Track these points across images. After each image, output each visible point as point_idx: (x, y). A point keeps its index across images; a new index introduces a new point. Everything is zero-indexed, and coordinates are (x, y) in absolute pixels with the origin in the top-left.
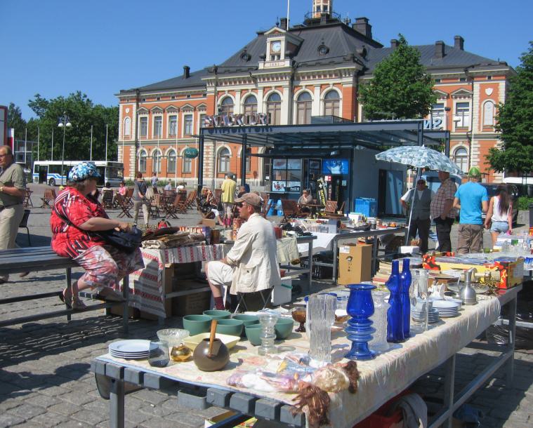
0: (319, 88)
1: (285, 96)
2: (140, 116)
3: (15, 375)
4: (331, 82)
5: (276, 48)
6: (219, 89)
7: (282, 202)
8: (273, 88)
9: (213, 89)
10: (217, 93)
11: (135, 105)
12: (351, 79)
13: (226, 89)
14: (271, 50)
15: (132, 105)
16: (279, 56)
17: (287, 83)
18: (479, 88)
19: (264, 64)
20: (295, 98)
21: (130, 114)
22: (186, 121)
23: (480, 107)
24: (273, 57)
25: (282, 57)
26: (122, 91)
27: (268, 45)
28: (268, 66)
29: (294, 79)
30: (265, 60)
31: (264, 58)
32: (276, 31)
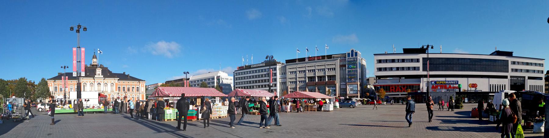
5: (99, 73)
11: (53, 83)
16: (100, 75)
24: (98, 75)
25: (101, 75)
27: (97, 72)
31: (96, 75)
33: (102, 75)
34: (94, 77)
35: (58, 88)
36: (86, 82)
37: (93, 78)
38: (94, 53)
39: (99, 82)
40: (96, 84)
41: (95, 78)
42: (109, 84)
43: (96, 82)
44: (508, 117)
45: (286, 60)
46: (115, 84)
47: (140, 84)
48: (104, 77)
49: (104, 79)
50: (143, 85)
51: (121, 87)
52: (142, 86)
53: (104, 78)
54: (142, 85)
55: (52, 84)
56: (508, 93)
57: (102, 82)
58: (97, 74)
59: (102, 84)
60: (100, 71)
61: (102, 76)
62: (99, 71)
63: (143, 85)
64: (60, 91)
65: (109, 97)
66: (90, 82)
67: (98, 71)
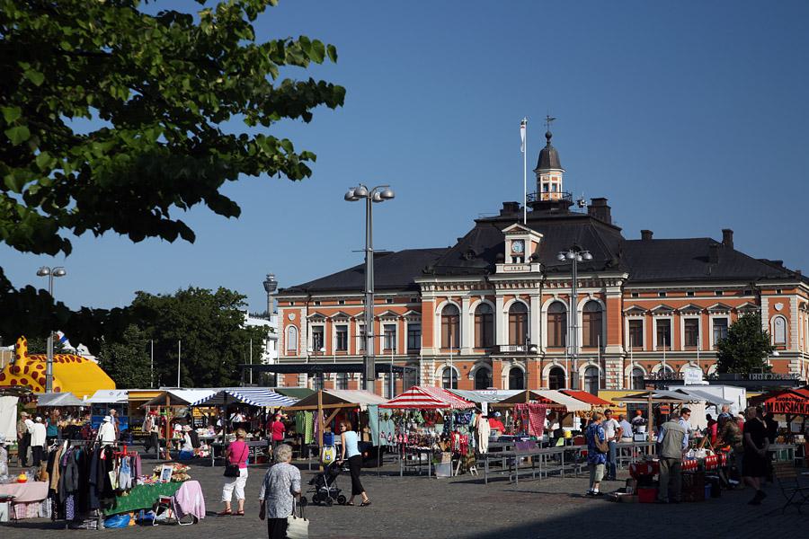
11: (304, 310)
31: (503, 261)
38: (548, 137)
43: (500, 302)
45: (642, 231)
47: (765, 300)
48: (542, 272)
52: (773, 310)
55: (298, 316)
58: (509, 260)
61: (536, 268)
62: (524, 244)
64: (660, 343)
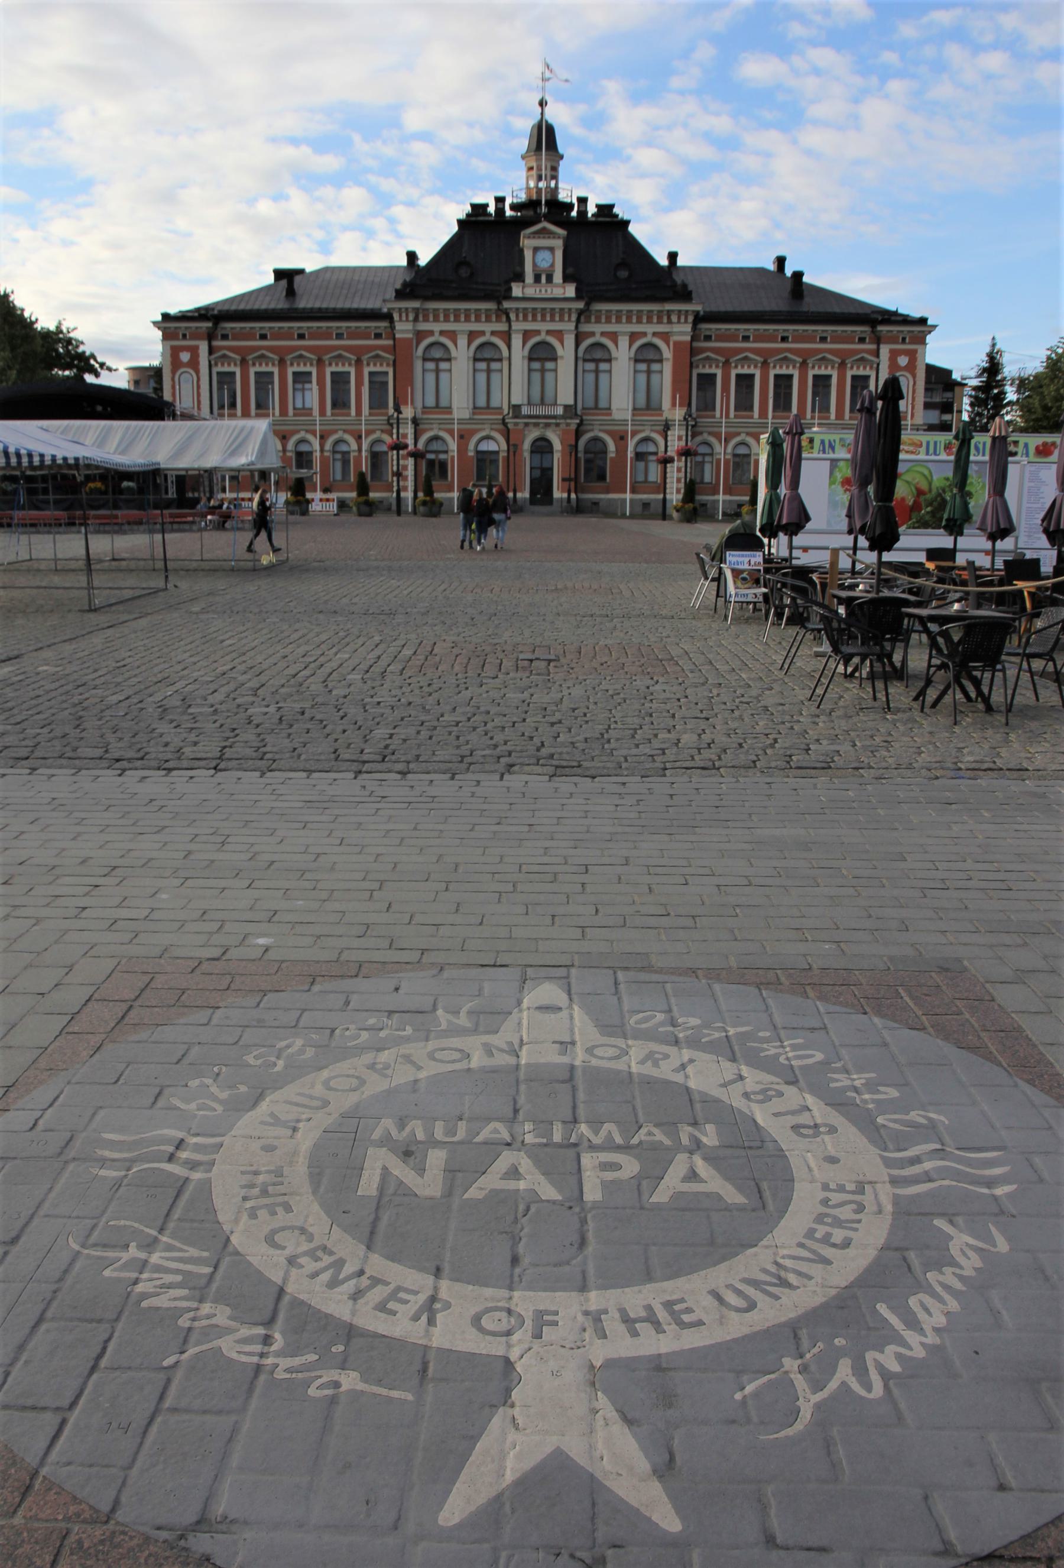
0: (627, 338)
1: (566, 351)
2: (215, 370)
3: (1010, 1183)
4: (650, 329)
5: (544, 260)
6: (423, 326)
7: (497, 512)
8: (488, 334)
9: (409, 326)
10: (420, 335)
11: (203, 347)
12: (688, 328)
13: (437, 327)
14: (534, 265)
15: (197, 348)
16: (550, 278)
17: (571, 326)
18: (888, 355)
19: (523, 288)
20: (580, 354)
21: (194, 364)
22: (853, 387)
23: (173, 380)
24: (537, 279)
25: (558, 277)
26: (166, 317)
27: (528, 255)
28: (530, 292)
29: (582, 316)
30: (523, 281)
31: (520, 277)
32: (544, 229)
33: (567, 278)
34: (499, 294)
35: (834, 381)
36: (549, 332)
37: (491, 306)
39: (598, 338)
40: (519, 351)
41: (506, 305)
42: (623, 353)
43: (517, 340)
44: (745, 1201)
46: (667, 353)
47: (885, 350)
48: (579, 296)
49: (580, 313)
50: (185, 357)
51: (719, 373)
53: (581, 305)
54: (894, 355)
55: (194, 351)
56: (973, 562)
57: (570, 340)
58: (529, 278)
59: (566, 351)
60: (552, 249)
61: (570, 291)
63: (185, 357)
64: (335, 405)
65: (621, 450)
66: (472, 335)
67: (536, 250)
